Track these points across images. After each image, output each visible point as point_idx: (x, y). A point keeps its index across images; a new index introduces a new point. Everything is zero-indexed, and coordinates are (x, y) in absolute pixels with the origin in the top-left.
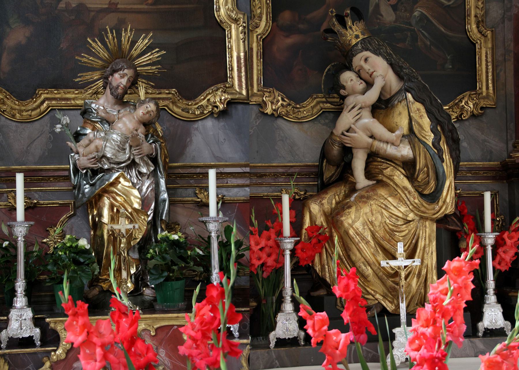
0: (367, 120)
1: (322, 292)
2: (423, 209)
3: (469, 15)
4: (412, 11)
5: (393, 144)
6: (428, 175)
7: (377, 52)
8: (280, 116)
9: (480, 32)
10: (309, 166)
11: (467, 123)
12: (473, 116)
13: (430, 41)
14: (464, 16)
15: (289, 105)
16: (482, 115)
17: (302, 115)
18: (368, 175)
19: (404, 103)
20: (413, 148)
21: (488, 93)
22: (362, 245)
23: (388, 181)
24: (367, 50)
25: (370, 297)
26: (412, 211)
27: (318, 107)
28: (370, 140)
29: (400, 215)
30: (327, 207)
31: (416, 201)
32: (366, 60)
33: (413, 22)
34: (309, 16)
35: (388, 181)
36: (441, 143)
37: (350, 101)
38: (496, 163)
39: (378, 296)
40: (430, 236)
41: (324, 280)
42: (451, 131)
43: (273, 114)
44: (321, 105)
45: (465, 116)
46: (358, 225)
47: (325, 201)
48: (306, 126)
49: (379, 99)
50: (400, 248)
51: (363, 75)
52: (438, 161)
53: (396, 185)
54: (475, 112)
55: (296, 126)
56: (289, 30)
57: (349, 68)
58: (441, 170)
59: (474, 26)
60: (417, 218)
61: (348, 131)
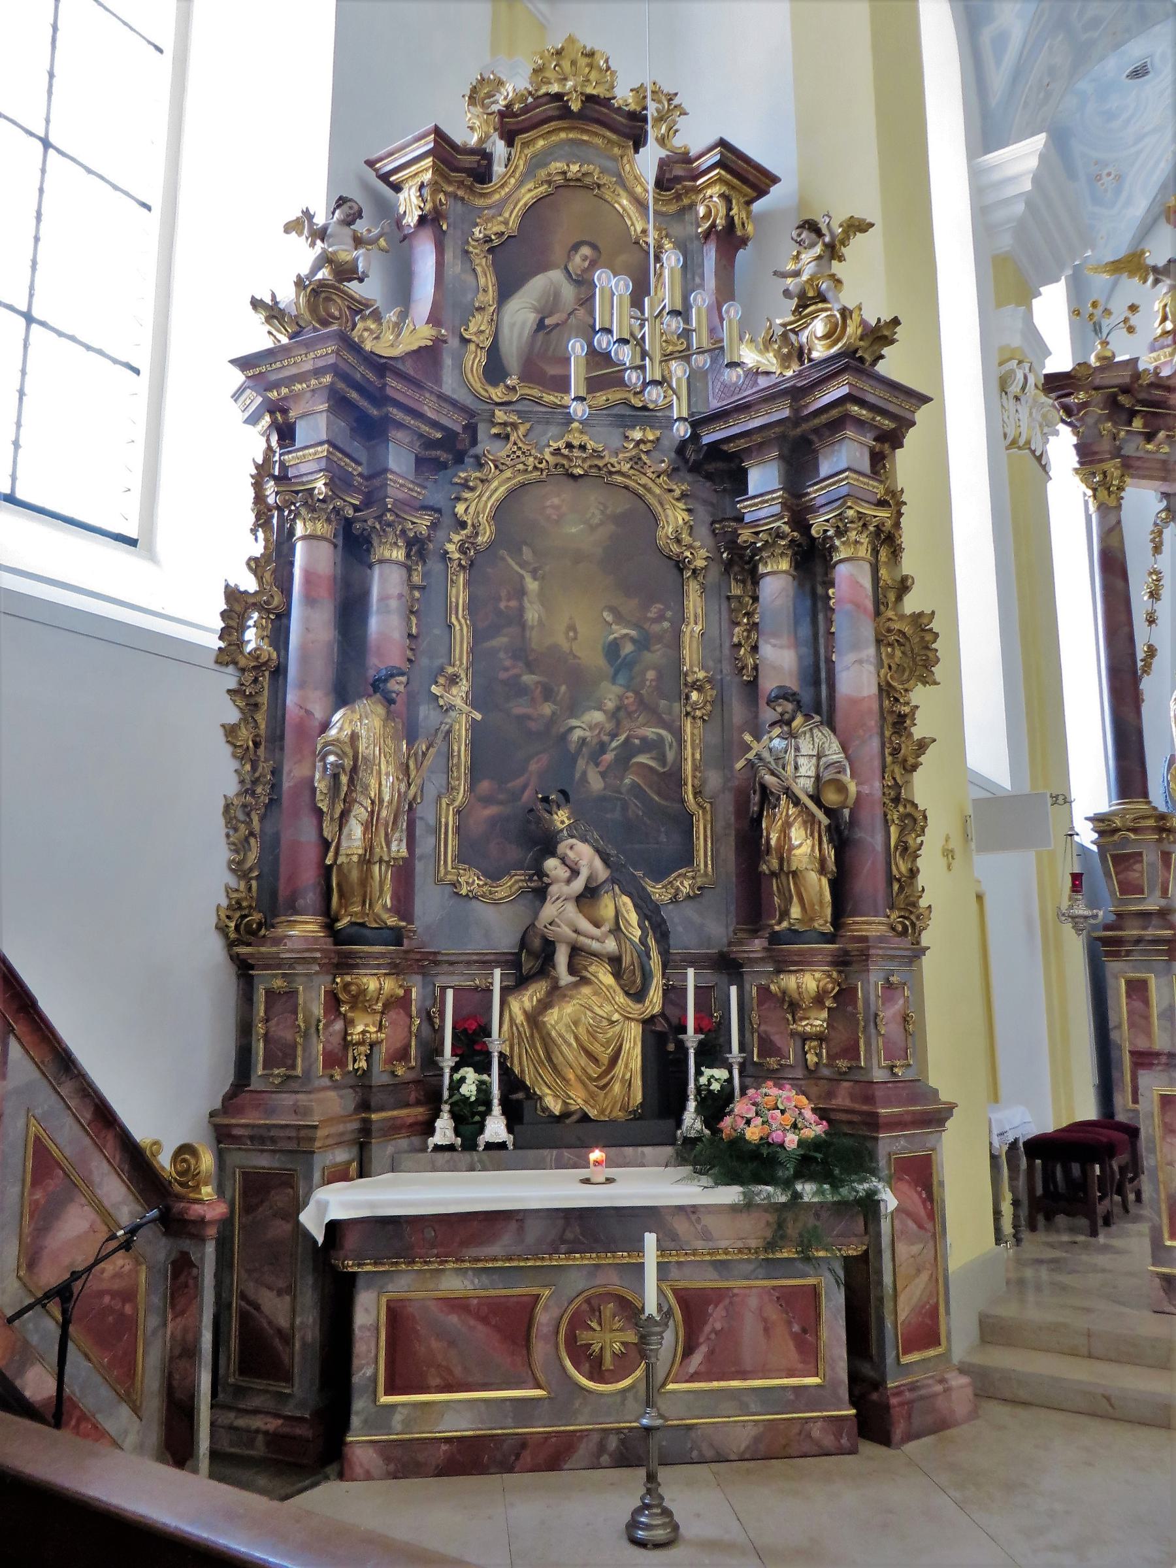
0: (571, 909)
1: (520, 1095)
2: (628, 1009)
3: (686, 784)
4: (622, 779)
5: (598, 940)
6: (634, 974)
7: (584, 840)
8: (476, 897)
9: (698, 804)
10: (504, 953)
11: (684, 904)
12: (688, 897)
13: (643, 812)
14: (680, 783)
15: (486, 884)
16: (696, 896)
17: (500, 896)
18: (572, 970)
19: (610, 894)
20: (619, 945)
21: (706, 871)
22: (564, 1048)
23: (593, 978)
24: (572, 837)
25: (571, 1101)
26: (617, 1011)
27: (516, 887)
28: (574, 935)
29: (605, 1015)
30: (528, 1005)
31: (622, 1000)
32: (571, 848)
33: (624, 790)
34: (510, 785)
35: (593, 978)
36: (649, 939)
37: (553, 889)
38: (714, 951)
39: (579, 1101)
40: (635, 1038)
41: (524, 1083)
42: (659, 926)
43: (467, 895)
44: (521, 884)
45: (681, 897)
46: (561, 1027)
47: (526, 999)
48: (503, 906)
49: (586, 888)
50: (748, 738)
51: (568, 862)
52: (645, 959)
53: (601, 982)
54: (691, 894)
55: (491, 907)
56: (487, 800)
57: (553, 854)
58: (648, 968)
59: (691, 796)
60: (622, 1019)
61: (550, 924)
